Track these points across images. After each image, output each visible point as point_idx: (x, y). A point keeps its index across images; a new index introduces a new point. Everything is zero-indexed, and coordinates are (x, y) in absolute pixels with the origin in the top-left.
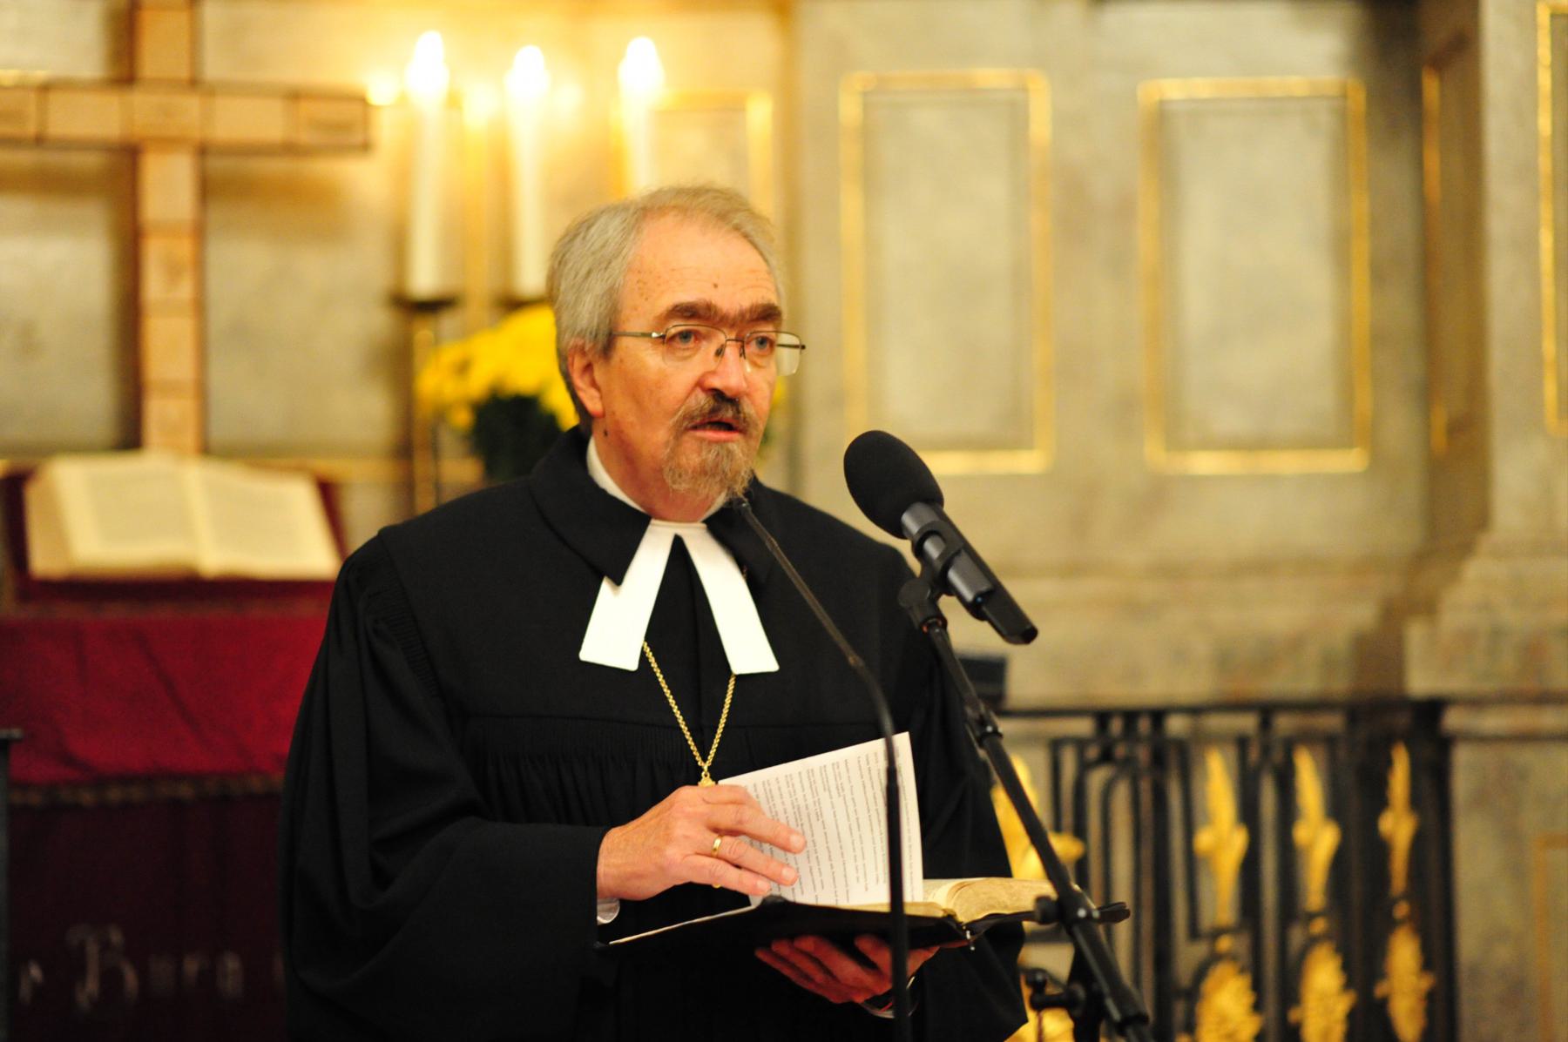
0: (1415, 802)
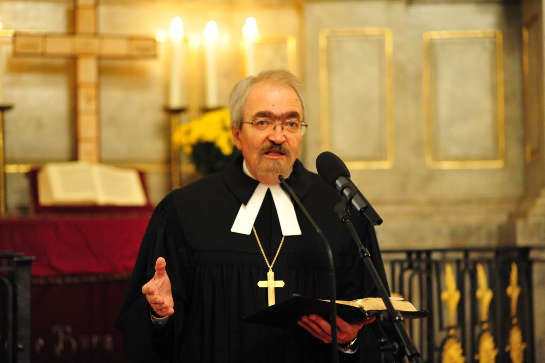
0: (520, 283)
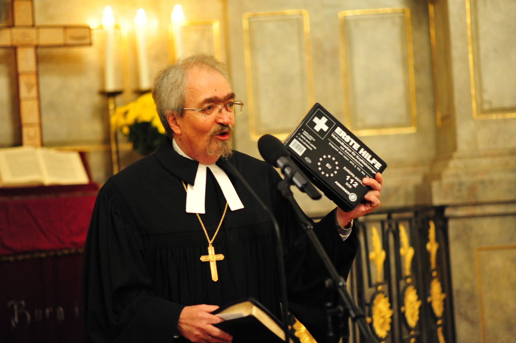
0: (437, 239)
